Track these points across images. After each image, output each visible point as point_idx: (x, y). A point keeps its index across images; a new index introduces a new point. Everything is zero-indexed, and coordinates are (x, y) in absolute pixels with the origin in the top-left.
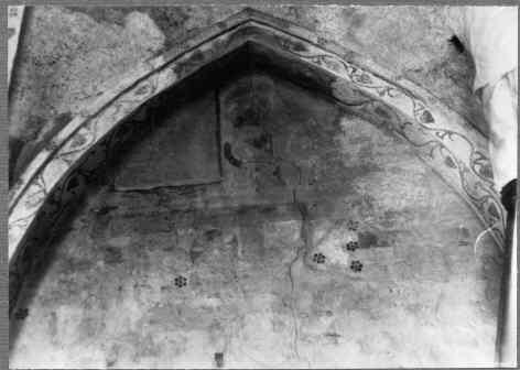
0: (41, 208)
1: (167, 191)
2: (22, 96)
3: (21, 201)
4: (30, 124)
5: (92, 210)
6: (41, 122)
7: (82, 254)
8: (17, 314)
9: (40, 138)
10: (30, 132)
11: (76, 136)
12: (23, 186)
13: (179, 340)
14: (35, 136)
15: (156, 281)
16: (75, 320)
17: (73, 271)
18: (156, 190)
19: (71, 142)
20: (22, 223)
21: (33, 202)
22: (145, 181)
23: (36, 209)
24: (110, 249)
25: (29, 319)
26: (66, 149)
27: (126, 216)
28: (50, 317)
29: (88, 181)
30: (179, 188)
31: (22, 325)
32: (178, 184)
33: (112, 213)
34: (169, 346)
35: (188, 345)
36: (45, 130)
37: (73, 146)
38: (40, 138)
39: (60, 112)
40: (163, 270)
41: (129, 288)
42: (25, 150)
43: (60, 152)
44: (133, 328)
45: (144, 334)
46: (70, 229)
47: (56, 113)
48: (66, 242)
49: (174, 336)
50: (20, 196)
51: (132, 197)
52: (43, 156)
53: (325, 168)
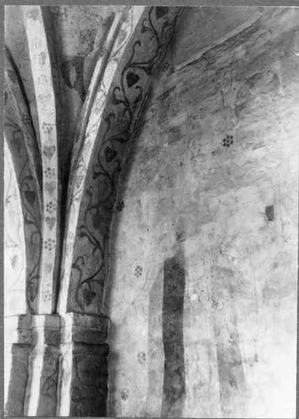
0: (105, 110)
1: (213, 52)
2: (66, 16)
3: (93, 109)
4: (83, 39)
5: (158, 98)
6: (91, 33)
7: (154, 141)
8: (118, 207)
9: (96, 48)
10: (86, 46)
11: (120, 33)
12: (90, 96)
13: (231, 201)
14: (91, 46)
15: (207, 147)
16: (154, 203)
17: (148, 159)
18: (203, 58)
19: (117, 42)
20: (94, 128)
21: (99, 108)
22: (194, 52)
23: (101, 113)
24: (173, 130)
25: (125, 209)
26: (115, 49)
27: (183, 92)
28: (136, 205)
29: (149, 71)
30: (223, 45)
31: (121, 216)
32: (222, 41)
33: (172, 94)
34: (222, 208)
35: (240, 204)
36: (97, 39)
37: (119, 43)
38: (96, 48)
39: (104, 17)
40: (213, 134)
41: (188, 163)
42: (87, 65)
43: (112, 54)
44: (193, 199)
45: (202, 203)
46: (145, 122)
47: (102, 19)
48: (143, 135)
49: (223, 198)
50: (91, 106)
51: (185, 72)
52: (99, 63)
53: (80, 13)
